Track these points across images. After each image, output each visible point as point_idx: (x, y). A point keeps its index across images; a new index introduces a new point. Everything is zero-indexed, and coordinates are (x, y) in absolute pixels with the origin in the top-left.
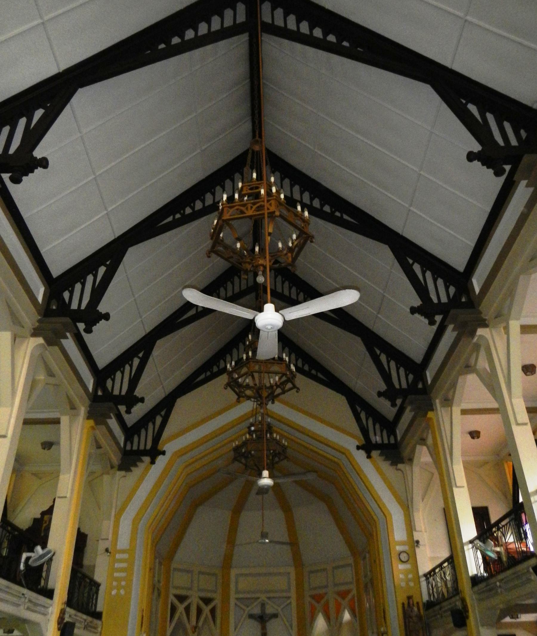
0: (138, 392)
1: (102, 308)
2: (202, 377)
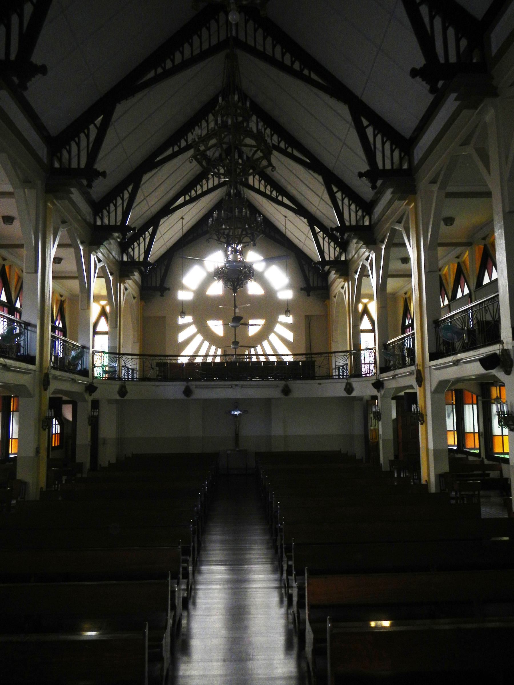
0: (99, 166)
1: (37, 58)
2: (169, 152)
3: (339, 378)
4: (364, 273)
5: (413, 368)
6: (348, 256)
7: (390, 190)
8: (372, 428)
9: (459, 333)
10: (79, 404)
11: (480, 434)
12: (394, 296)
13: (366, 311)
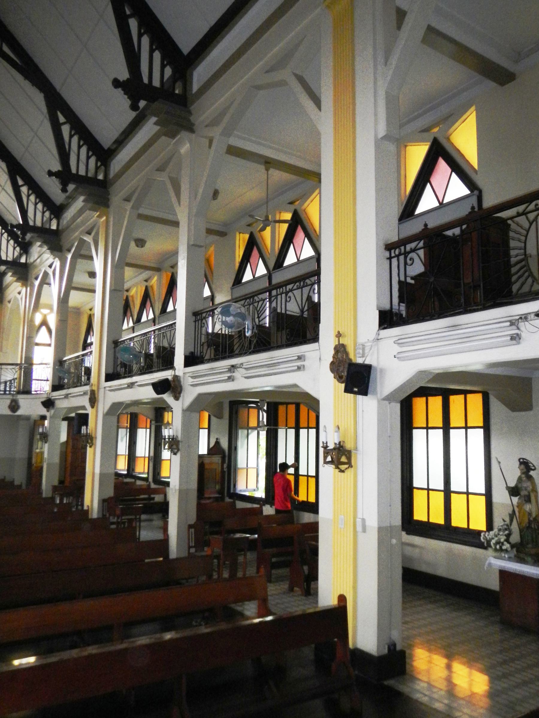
3: (5, 394)
4: (45, 281)
5: (87, 388)
6: (30, 259)
7: (82, 198)
8: (38, 451)
9: (137, 356)
10: (397, 520)
11: (150, 458)
12: (78, 311)
13: (44, 323)
